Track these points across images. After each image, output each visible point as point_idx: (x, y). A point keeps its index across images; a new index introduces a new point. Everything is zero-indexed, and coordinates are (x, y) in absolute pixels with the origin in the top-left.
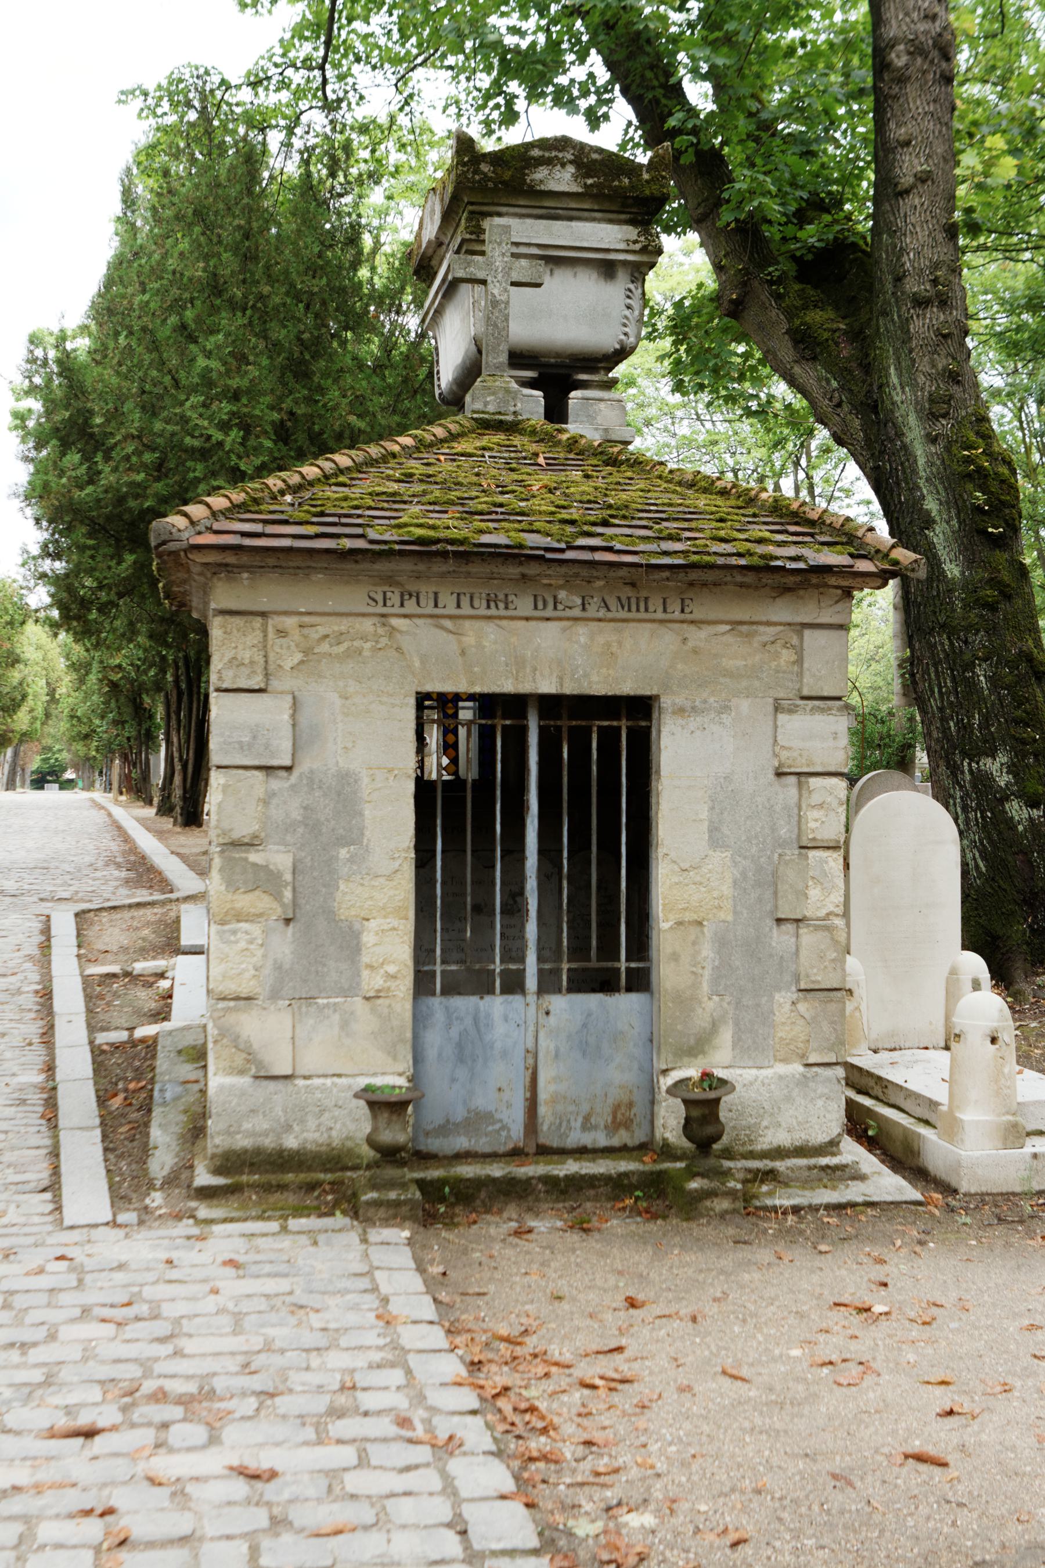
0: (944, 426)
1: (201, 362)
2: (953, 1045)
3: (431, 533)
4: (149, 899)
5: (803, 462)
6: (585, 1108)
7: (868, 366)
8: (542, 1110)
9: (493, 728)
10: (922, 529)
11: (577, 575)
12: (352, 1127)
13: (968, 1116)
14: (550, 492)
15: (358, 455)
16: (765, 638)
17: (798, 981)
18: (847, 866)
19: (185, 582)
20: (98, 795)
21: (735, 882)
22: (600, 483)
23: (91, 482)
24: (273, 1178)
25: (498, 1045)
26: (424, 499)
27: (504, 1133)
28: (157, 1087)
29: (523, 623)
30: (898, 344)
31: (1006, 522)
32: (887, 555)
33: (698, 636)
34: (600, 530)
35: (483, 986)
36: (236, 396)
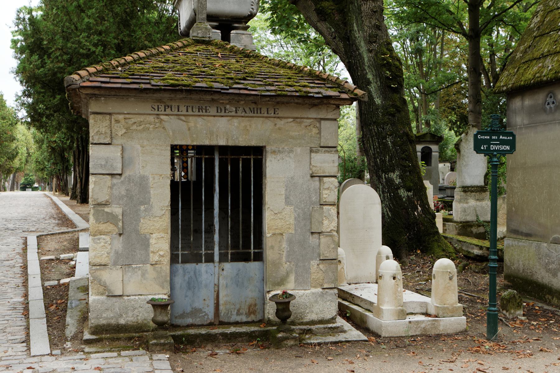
0: (375, 46)
1: (86, 20)
2: (379, 281)
3: (176, 82)
4: (67, 230)
5: (322, 63)
6: (238, 306)
7: (346, 23)
8: (221, 307)
9: (201, 159)
10: (366, 85)
11: (233, 99)
12: (146, 315)
13: (385, 307)
14: (223, 67)
15: (148, 53)
16: (307, 124)
17: (320, 256)
18: (338, 213)
19: (79, 102)
20: (47, 193)
21: (295, 218)
22: (242, 64)
23: (42, 67)
24: (115, 336)
25: (204, 282)
26: (173, 69)
27: (206, 317)
28: (69, 302)
29: (213, 118)
30: (357, 15)
31: (398, 83)
32: (353, 92)
33: (281, 123)
34: (242, 82)
35: (197, 259)
36: (100, 33)
